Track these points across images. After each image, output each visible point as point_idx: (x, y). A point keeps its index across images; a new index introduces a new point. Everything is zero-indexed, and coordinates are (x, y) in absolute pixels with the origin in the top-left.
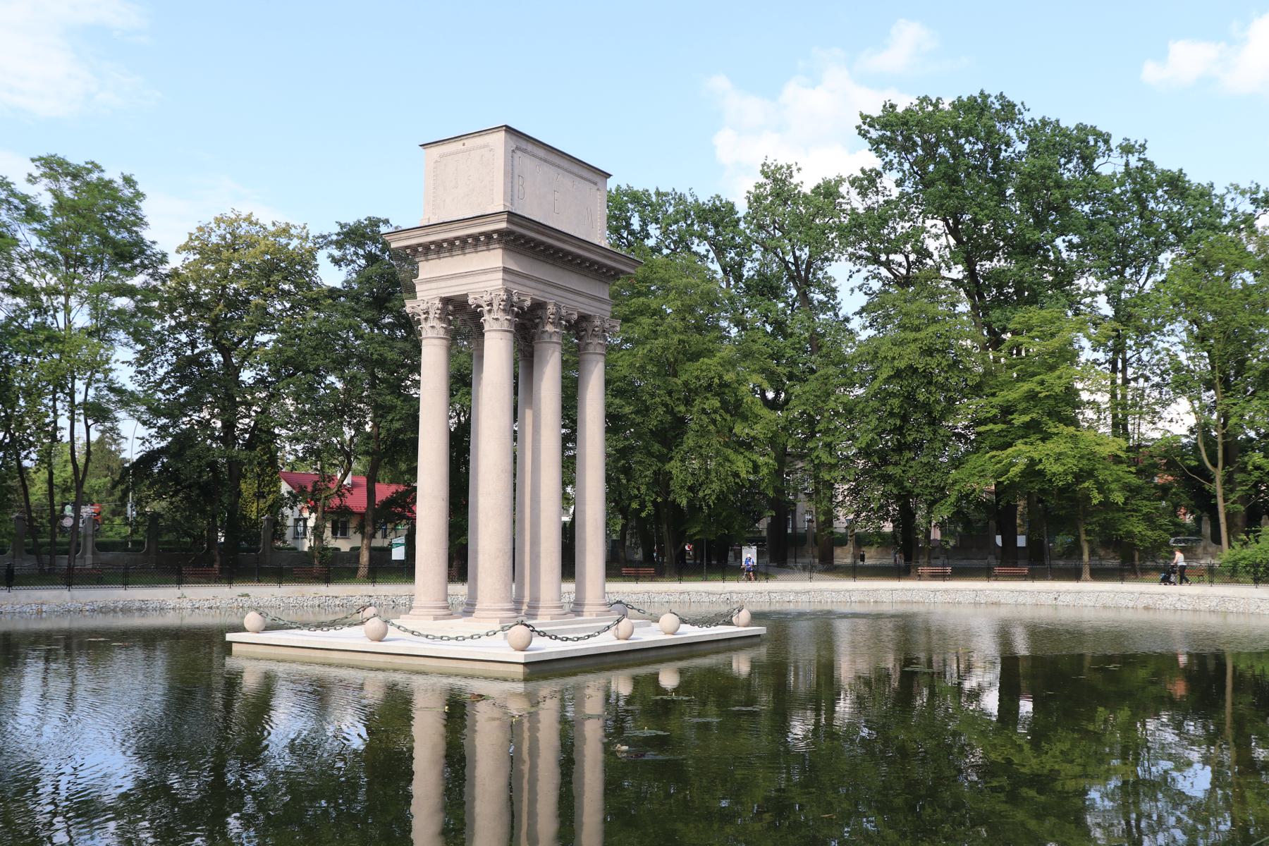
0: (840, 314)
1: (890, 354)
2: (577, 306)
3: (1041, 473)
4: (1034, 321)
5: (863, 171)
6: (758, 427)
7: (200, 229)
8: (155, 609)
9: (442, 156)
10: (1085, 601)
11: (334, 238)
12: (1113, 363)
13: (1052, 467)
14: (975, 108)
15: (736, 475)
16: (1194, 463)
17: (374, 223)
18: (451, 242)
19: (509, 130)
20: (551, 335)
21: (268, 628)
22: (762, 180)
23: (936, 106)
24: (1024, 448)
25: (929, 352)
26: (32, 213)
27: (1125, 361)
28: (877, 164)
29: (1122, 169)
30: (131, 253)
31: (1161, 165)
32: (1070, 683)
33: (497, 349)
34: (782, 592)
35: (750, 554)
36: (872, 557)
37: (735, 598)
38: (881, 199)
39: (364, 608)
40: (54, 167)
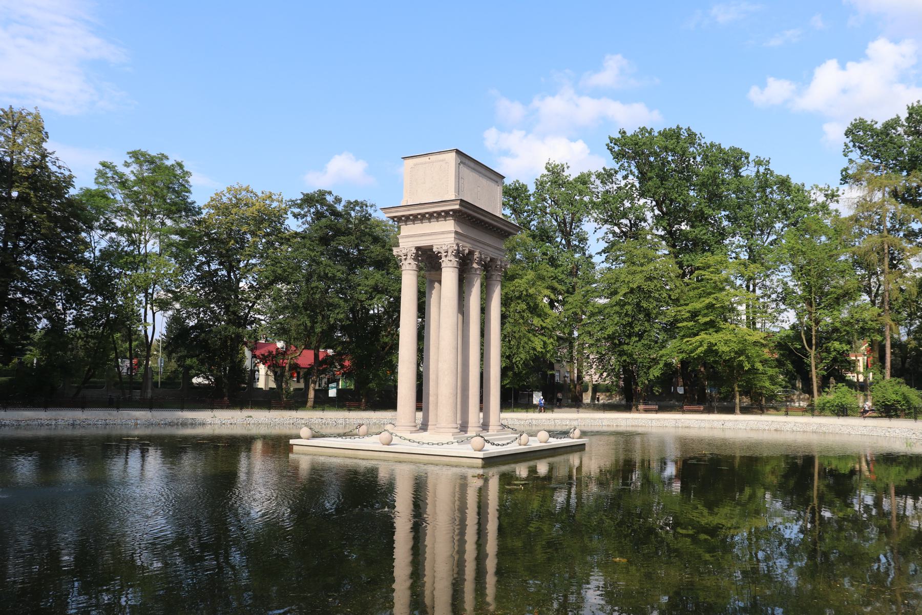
0: (587, 253)
1: (627, 280)
2: (491, 253)
3: (716, 352)
4: (711, 263)
5: (604, 169)
6: (548, 321)
7: (216, 194)
8: (200, 424)
9: (415, 165)
10: (740, 426)
11: (299, 202)
12: (748, 287)
13: (723, 348)
14: (672, 135)
15: (534, 349)
16: (799, 347)
17: (322, 194)
18: (423, 215)
19: (458, 152)
20: (476, 269)
21: (314, 437)
22: (546, 172)
23: (650, 133)
24: (705, 336)
25: (650, 279)
26: (123, 184)
27: (754, 286)
28: (617, 167)
29: (753, 174)
30: (184, 208)
31: (777, 172)
32: (713, 475)
33: (449, 275)
34: (562, 419)
35: (537, 398)
36: (603, 399)
37: (534, 422)
38: (615, 187)
39: (360, 425)
40: (137, 156)
